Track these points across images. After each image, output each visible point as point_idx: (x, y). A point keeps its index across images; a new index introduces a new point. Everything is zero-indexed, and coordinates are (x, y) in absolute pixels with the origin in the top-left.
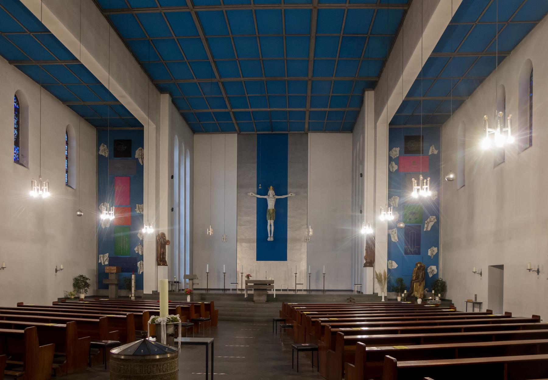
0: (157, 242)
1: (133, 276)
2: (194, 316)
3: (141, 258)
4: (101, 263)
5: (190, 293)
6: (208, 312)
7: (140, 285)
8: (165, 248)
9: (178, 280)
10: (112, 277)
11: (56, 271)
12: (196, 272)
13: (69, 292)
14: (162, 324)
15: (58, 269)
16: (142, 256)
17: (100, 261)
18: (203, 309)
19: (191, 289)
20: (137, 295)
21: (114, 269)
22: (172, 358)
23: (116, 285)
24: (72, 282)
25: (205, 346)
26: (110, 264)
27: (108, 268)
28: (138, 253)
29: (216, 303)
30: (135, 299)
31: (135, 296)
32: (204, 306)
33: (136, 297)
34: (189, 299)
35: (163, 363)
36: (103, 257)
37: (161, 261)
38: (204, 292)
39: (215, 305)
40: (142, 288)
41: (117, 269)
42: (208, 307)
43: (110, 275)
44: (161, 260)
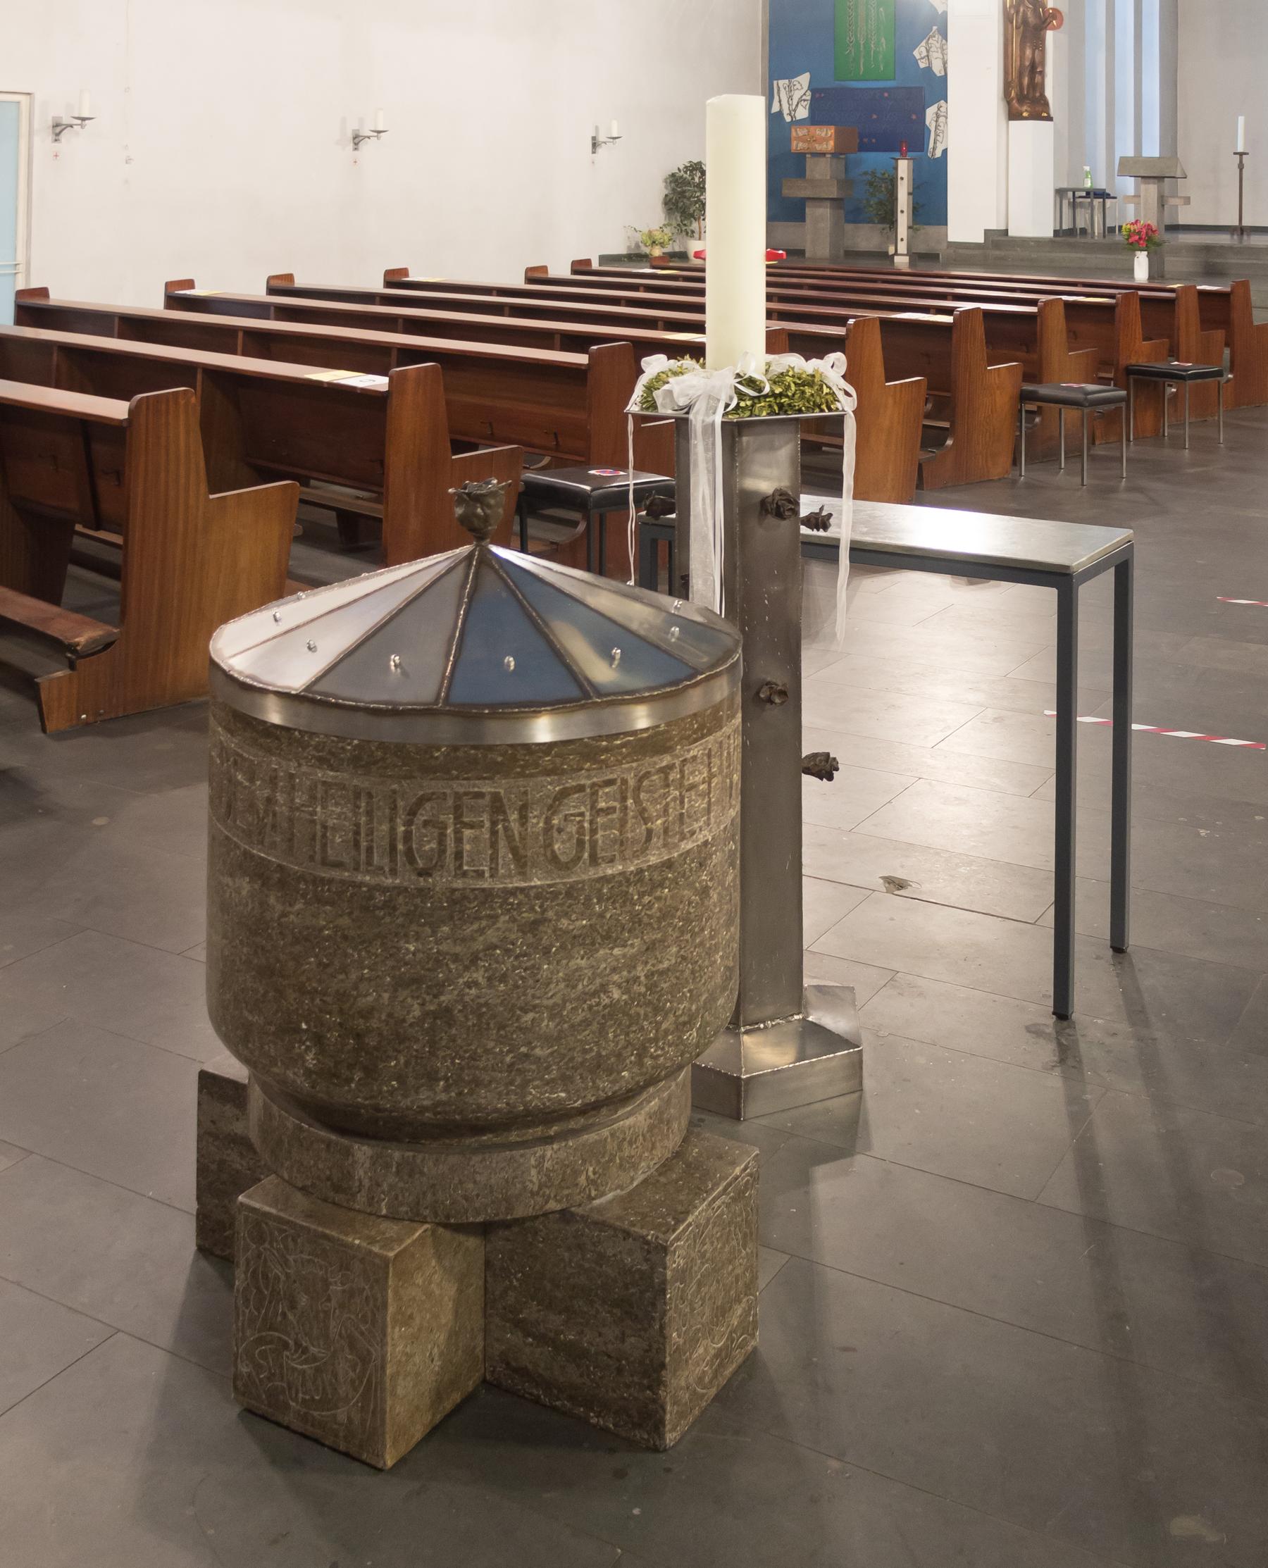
0: (1007, 19)
1: (904, 167)
2: (1140, 351)
3: (936, 88)
4: (780, 113)
5: (1144, 239)
6: (1219, 335)
7: (931, 205)
8: (1039, 44)
9: (1102, 185)
10: (820, 171)
11: (595, 145)
12: (1193, 157)
13: (646, 231)
14: (697, 419)
15: (601, 138)
16: (944, 79)
17: (775, 108)
18: (1188, 317)
19: (1153, 222)
20: (922, 248)
21: (826, 138)
22: (653, 743)
23: (836, 202)
24: (658, 191)
25: (1048, 596)
26: (816, 118)
27: (801, 132)
28: (929, 69)
29: (1258, 293)
30: (911, 263)
31: (910, 253)
32: (1193, 302)
33: (915, 257)
34: (1141, 270)
35: (552, 787)
36: (790, 89)
37: (1022, 98)
38: (1224, 239)
39: (1255, 298)
40: (941, 218)
41: (839, 136)
42: (1219, 310)
43: (810, 162)
44: (1024, 97)
